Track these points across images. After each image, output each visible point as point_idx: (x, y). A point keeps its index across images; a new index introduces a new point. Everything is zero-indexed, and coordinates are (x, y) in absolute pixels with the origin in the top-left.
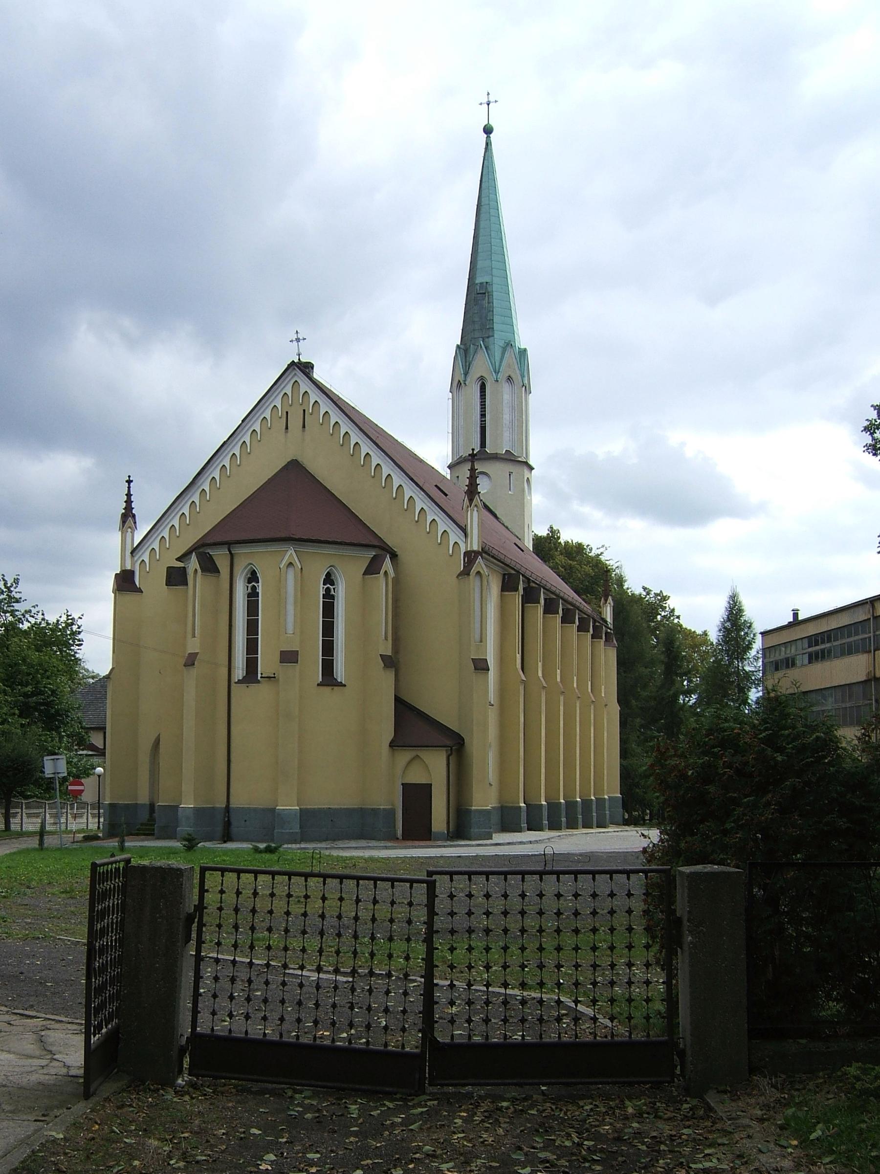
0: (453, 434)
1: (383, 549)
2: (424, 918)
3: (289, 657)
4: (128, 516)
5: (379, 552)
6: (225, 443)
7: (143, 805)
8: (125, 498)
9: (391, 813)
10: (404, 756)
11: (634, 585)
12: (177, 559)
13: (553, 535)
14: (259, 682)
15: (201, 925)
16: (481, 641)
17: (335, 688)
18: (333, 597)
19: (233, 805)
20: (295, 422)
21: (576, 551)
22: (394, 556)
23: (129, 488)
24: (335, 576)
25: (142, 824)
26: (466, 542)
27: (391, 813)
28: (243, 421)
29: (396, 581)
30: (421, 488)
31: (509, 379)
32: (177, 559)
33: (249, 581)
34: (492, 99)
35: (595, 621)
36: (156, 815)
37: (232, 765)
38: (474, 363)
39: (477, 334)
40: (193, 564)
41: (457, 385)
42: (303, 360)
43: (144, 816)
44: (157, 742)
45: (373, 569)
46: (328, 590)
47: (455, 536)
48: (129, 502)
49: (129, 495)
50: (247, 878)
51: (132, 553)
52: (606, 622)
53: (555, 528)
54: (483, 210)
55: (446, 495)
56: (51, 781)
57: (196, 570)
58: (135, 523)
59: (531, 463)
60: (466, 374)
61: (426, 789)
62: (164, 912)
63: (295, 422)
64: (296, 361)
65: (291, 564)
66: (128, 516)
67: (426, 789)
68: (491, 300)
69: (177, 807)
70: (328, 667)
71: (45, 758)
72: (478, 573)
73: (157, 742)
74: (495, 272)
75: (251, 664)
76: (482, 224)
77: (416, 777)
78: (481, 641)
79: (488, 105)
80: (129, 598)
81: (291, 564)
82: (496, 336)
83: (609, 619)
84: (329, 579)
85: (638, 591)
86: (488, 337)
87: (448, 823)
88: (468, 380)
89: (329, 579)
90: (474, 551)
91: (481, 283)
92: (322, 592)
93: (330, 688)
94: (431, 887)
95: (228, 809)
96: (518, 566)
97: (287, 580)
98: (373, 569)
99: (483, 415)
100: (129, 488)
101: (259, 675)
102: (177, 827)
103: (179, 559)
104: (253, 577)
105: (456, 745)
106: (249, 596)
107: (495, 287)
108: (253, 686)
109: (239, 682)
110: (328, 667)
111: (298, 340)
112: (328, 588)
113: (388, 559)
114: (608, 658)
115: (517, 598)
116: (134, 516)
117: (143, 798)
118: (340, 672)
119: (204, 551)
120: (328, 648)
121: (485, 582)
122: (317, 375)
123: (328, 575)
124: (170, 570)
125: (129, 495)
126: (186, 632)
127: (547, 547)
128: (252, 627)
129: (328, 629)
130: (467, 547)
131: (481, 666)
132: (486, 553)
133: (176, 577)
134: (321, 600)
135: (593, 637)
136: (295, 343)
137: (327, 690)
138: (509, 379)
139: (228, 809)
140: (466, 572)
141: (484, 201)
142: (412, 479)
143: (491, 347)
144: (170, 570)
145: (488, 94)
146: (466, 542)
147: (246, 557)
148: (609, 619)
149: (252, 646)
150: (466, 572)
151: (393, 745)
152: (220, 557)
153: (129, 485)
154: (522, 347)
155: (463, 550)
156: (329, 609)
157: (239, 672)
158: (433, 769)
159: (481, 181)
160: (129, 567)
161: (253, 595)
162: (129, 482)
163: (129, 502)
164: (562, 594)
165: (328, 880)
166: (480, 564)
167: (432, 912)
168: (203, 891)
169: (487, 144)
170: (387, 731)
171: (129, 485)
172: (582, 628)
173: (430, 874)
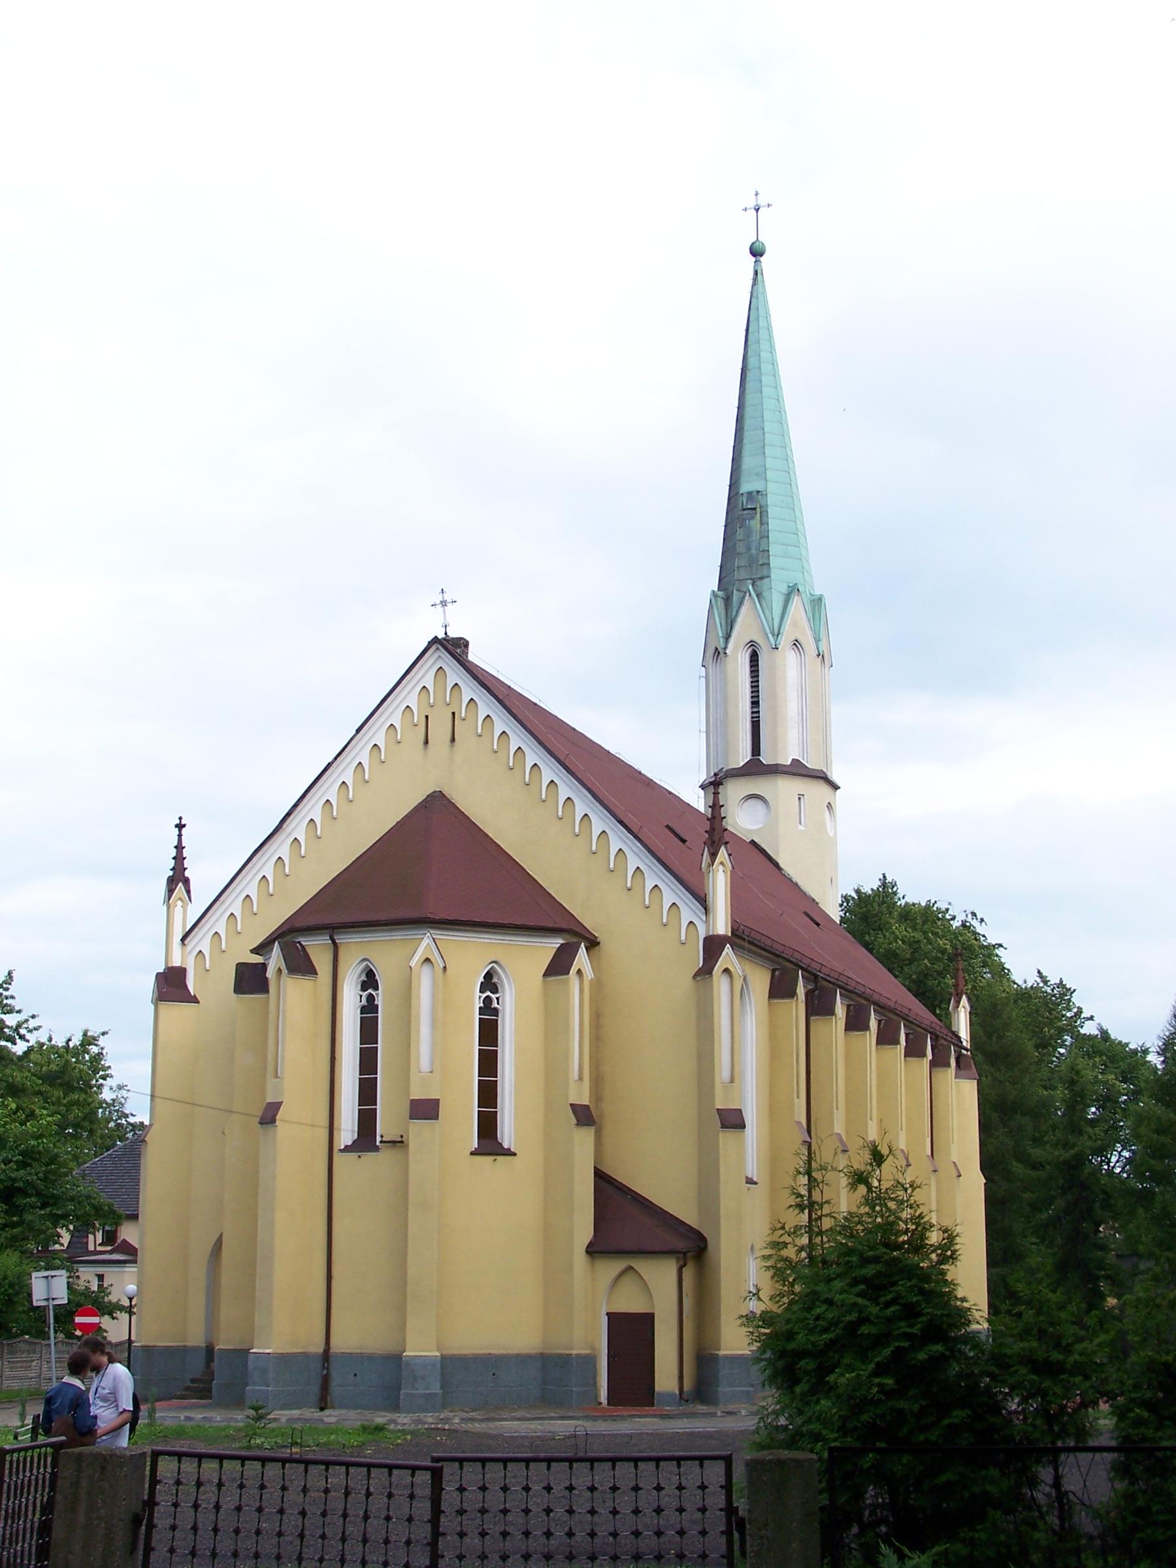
0: (707, 732)
1: (576, 934)
2: (427, 1516)
3: (425, 1110)
4: (178, 878)
5: (572, 938)
6: (329, 765)
7: (195, 1349)
8: (174, 852)
9: (589, 1361)
10: (610, 1268)
11: (1022, 969)
12: (251, 951)
13: (886, 890)
14: (377, 1149)
15: (151, 1526)
16: (732, 1081)
17: (499, 1158)
18: (495, 1012)
19: (337, 1345)
20: (440, 731)
21: (927, 918)
22: (593, 944)
23: (180, 836)
24: (499, 978)
25: (193, 1381)
26: (707, 922)
27: (589, 1361)
28: (358, 731)
29: (598, 986)
30: (636, 837)
31: (796, 644)
32: (251, 951)
33: (364, 987)
34: (762, 201)
35: (935, 1038)
36: (215, 1365)
37: (334, 1283)
38: (740, 619)
39: (743, 574)
40: (275, 960)
41: (716, 654)
42: (453, 634)
43: (196, 1367)
44: (219, 1244)
45: (559, 966)
46: (488, 1000)
47: (689, 911)
48: (179, 859)
49: (179, 847)
50: (210, 1466)
51: (183, 940)
52: (959, 1038)
53: (889, 879)
54: (750, 376)
55: (684, 841)
56: (43, 1310)
57: (280, 970)
58: (188, 892)
59: (835, 777)
60: (727, 638)
61: (646, 1321)
62: (102, 1511)
63: (440, 731)
64: (441, 635)
65: (427, 960)
66: (178, 878)
67: (646, 1321)
68: (764, 519)
69: (246, 1352)
70: (488, 1126)
71: (34, 1275)
72: (726, 971)
73: (219, 1244)
74: (770, 474)
75: (367, 1120)
76: (750, 398)
77: (630, 1302)
78: (732, 1081)
79: (757, 210)
80: (175, 1012)
81: (427, 960)
82: (773, 576)
83: (964, 1033)
84: (490, 983)
85: (1032, 980)
86: (761, 578)
87: (681, 1377)
88: (730, 645)
89: (490, 983)
90: (719, 936)
91: (750, 493)
92: (478, 1004)
93: (492, 1158)
94: (437, 1475)
95: (326, 1355)
96: (796, 955)
97: (436, 976)
98: (559, 966)
99: (755, 703)
100: (180, 836)
101: (378, 1139)
102: (247, 1385)
103: (256, 951)
104: (370, 981)
105: (692, 1248)
106: (363, 1010)
107: (771, 500)
108: (369, 1157)
109: (347, 1149)
110: (488, 1126)
111: (444, 603)
112: (488, 997)
113: (582, 950)
114: (962, 1098)
115: (797, 1007)
116: (186, 882)
117: (196, 1338)
118: (507, 1134)
119: (294, 940)
120: (488, 1094)
121: (738, 983)
122: (473, 656)
123: (489, 976)
124: (242, 968)
125: (179, 847)
126: (265, 1068)
127: (873, 912)
128: (368, 1061)
129: (488, 1063)
130: (708, 929)
131: (733, 1121)
132: (739, 937)
133: (250, 980)
134: (477, 1016)
135: (934, 1064)
136: (439, 607)
137: (488, 1160)
138: (796, 644)
139: (326, 1355)
140: (706, 971)
141: (752, 362)
142: (621, 822)
143: (766, 594)
144: (242, 968)
145: (757, 194)
146: (707, 922)
147: (357, 951)
148: (964, 1033)
149: (367, 1092)
150: (706, 971)
151: (594, 1251)
152: (317, 948)
153: (180, 831)
154: (817, 593)
155: (702, 934)
156: (489, 1031)
157: (347, 1131)
158: (658, 1287)
159: (747, 330)
160: (176, 962)
161: (369, 1009)
162: (180, 826)
163: (179, 859)
164: (876, 997)
165: (352, 1470)
166: (728, 957)
167: (437, 1511)
168: (154, 1481)
169: (756, 273)
170: (584, 1229)
171: (180, 831)
172: (914, 1050)
173: (436, 1460)
